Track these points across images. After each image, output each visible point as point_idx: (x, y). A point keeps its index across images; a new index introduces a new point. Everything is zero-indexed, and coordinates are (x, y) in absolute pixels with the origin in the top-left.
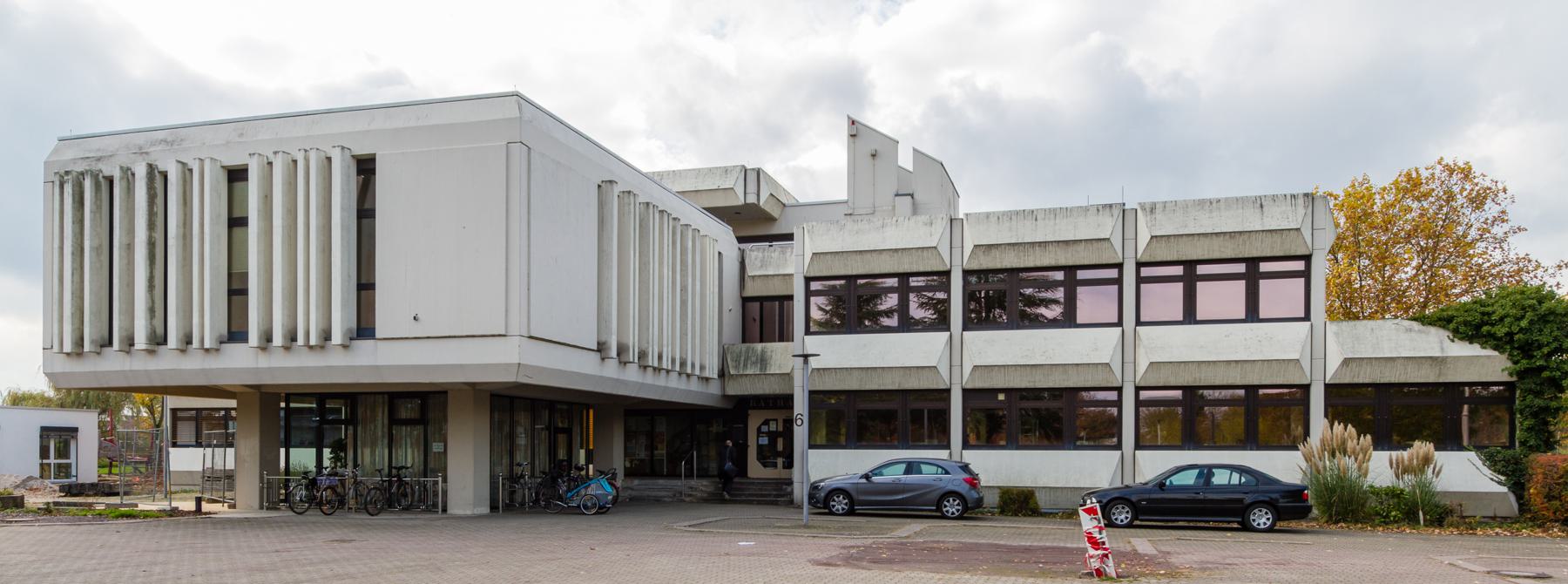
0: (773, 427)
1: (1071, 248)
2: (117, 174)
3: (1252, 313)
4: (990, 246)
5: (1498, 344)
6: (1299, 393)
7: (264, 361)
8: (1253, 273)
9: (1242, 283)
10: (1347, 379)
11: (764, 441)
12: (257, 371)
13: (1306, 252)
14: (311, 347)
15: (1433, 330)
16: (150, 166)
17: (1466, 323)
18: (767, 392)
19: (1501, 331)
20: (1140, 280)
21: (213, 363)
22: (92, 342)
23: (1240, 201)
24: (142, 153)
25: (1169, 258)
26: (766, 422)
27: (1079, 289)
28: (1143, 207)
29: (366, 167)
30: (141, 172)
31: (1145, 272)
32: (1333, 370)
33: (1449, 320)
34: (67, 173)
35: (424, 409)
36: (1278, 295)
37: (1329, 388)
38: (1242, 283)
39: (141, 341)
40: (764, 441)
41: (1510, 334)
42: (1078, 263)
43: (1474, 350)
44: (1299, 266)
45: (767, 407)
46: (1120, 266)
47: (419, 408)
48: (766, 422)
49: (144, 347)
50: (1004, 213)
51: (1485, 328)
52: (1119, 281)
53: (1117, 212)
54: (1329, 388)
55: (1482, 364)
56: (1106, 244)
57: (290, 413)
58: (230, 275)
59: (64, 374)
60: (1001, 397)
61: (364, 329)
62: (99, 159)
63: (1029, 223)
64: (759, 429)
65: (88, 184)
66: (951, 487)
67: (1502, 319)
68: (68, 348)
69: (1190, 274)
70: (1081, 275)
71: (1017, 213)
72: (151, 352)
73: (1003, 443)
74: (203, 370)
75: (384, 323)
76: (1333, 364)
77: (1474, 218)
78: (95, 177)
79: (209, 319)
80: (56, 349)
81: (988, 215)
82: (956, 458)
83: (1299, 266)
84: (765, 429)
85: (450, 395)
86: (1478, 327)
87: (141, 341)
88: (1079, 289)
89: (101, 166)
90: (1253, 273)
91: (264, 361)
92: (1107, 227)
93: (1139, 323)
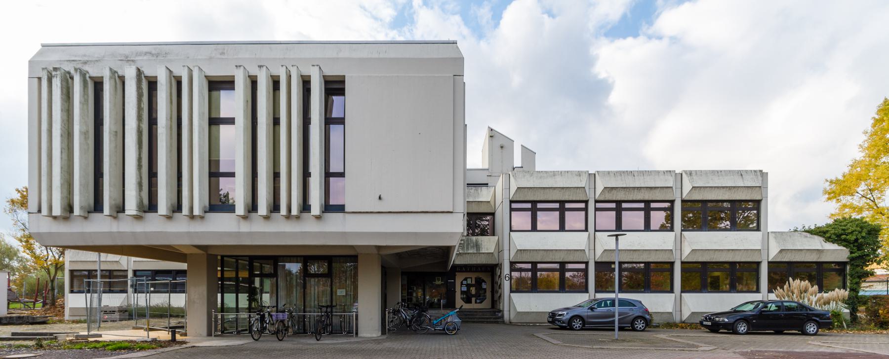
0: (469, 281)
1: (653, 191)
2: (106, 75)
3: (534, 228)
4: (612, 188)
5: (845, 243)
6: (755, 266)
7: (245, 227)
8: (562, 208)
9: (643, 212)
10: (604, 260)
11: (464, 289)
12: (238, 234)
13: (585, 199)
14: (55, 218)
15: (816, 237)
16: (139, 72)
17: (835, 234)
18: (475, 262)
20: (596, 209)
21: (139, 228)
22: (81, 208)
24: (128, 60)
25: (578, 199)
26: (466, 279)
27: (652, 212)
28: (686, 172)
30: (130, 74)
31: (514, 206)
32: (598, 257)
33: (825, 233)
34: (55, 69)
35: (330, 267)
36: (574, 219)
37: (597, 263)
38: (643, 212)
39: (131, 207)
40: (464, 289)
41: (856, 240)
42: (538, 199)
43: (830, 246)
44: (582, 205)
45: (466, 271)
46: (586, 202)
47: (334, 264)
48: (466, 279)
49: (135, 213)
50: (617, 172)
51: (844, 237)
52: (586, 210)
53: (673, 174)
54: (597, 263)
56: (670, 190)
57: (236, 269)
58: (210, 161)
59: (50, 234)
61: (328, 208)
62: (85, 63)
63: (630, 177)
64: (462, 284)
65: (77, 79)
66: (637, 315)
67: (852, 232)
68: (57, 211)
69: (619, 208)
70: (624, 205)
71: (624, 172)
72: (169, 217)
74: (188, 233)
76: (599, 252)
78: (83, 74)
79: (197, 194)
80: (45, 211)
81: (609, 172)
82: (592, 298)
83: (582, 205)
84: (465, 282)
85: (359, 258)
86: (839, 236)
87: (131, 207)
88: (652, 212)
89: (86, 68)
90: (562, 208)
91: (245, 227)
92: (582, 183)
93: (511, 230)
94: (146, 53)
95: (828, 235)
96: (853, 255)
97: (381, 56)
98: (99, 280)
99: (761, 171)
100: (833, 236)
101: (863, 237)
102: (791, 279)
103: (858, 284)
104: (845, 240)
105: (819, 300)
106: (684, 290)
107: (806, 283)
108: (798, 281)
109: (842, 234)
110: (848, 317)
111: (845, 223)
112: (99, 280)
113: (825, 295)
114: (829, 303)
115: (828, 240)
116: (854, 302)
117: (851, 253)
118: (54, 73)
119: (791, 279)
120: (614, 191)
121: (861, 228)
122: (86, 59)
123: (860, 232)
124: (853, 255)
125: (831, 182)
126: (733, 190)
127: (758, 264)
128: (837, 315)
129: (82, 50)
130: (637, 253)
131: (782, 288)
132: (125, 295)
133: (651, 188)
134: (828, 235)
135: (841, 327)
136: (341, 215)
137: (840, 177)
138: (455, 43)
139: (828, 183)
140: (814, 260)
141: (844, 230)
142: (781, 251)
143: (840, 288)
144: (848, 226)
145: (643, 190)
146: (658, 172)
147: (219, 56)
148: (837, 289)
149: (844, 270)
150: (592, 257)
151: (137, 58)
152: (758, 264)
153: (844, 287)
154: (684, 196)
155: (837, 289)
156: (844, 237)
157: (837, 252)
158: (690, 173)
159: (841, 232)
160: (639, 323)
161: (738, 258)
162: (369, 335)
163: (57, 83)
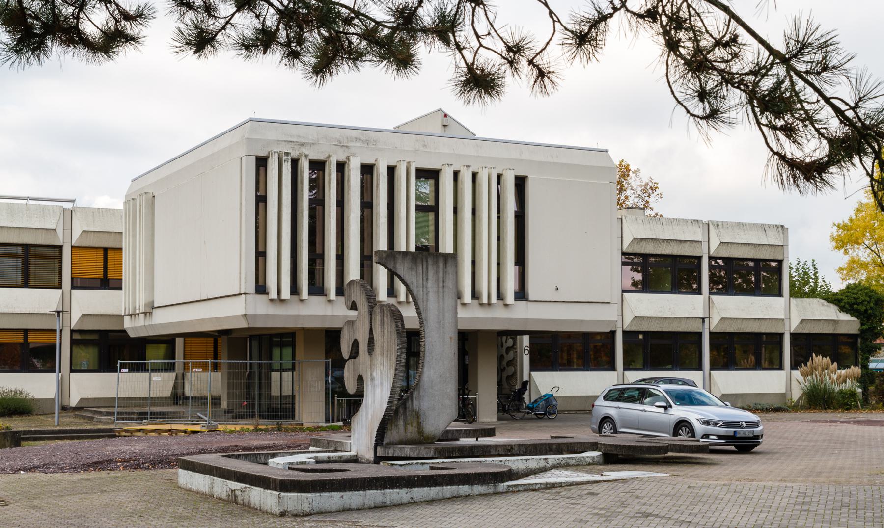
4: (642, 239)
13: (780, 258)
15: (832, 305)
17: (848, 303)
19: (863, 308)
23: (755, 226)
29: (521, 183)
32: (794, 325)
37: (792, 335)
41: (866, 310)
54: (792, 335)
55: (848, 323)
56: (699, 244)
60: (641, 337)
61: (521, 294)
70: (381, 244)
73: (17, 368)
75: (533, 291)
76: (628, 319)
77: (634, 217)
86: (851, 305)
92: (697, 234)
94: (356, 139)
95: (842, 304)
96: (864, 327)
97: (556, 160)
98: (248, 361)
99: (782, 226)
100: (847, 306)
101: (871, 308)
102: (814, 355)
103: (868, 359)
104: (857, 310)
105: (839, 377)
106: (713, 368)
107: (827, 360)
108: (820, 357)
109: (854, 304)
110: (861, 397)
111: (855, 291)
112: (248, 361)
113: (843, 372)
114: (845, 382)
115: (842, 309)
116: (868, 378)
117: (862, 324)
118: (285, 158)
119: (814, 355)
120: (643, 243)
121: (870, 297)
122: (302, 141)
123: (869, 302)
124: (864, 327)
125: (838, 226)
126: (758, 248)
127: (781, 335)
128: (853, 394)
129: (293, 130)
130: (668, 321)
131: (806, 365)
132: (60, 291)
133: (681, 241)
134: (842, 304)
135: (857, 407)
136: (524, 303)
137: (847, 221)
138: (607, 151)
139: (836, 228)
140: (831, 332)
141: (855, 299)
142: (803, 321)
143: (205, 368)
144: (859, 295)
145: (672, 244)
146: (686, 221)
147: (422, 149)
148: (852, 367)
149: (856, 343)
150: (619, 325)
151: (350, 144)
152: (781, 335)
153: (856, 364)
154: (711, 253)
155: (852, 367)
156: (855, 306)
157: (848, 323)
158: (717, 225)
159: (854, 301)
160: (249, 509)
161: (763, 330)
162: (488, 420)
163: (287, 168)
